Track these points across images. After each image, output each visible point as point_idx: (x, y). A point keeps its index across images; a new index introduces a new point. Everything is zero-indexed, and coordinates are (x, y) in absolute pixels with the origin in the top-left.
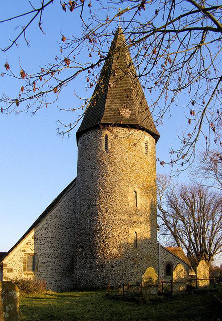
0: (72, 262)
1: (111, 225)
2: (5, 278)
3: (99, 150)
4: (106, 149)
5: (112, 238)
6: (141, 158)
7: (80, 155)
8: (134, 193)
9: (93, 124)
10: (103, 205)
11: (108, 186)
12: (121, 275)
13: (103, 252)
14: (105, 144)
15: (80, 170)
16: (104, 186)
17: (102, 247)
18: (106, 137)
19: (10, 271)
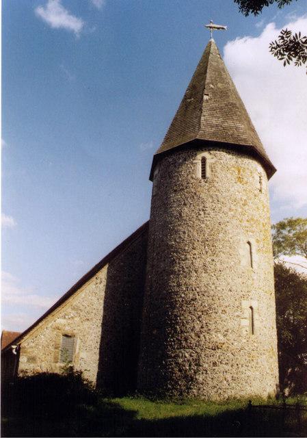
0: (70, 337)
1: (212, 293)
2: (22, 371)
3: (192, 178)
4: (204, 176)
5: (214, 315)
6: (255, 196)
7: (155, 198)
8: (248, 246)
9: (168, 165)
10: (198, 260)
11: (207, 231)
12: (230, 379)
13: (199, 337)
14: (202, 168)
15: (152, 214)
16: (201, 231)
17: (197, 328)
18: (204, 160)
19: (32, 359)
